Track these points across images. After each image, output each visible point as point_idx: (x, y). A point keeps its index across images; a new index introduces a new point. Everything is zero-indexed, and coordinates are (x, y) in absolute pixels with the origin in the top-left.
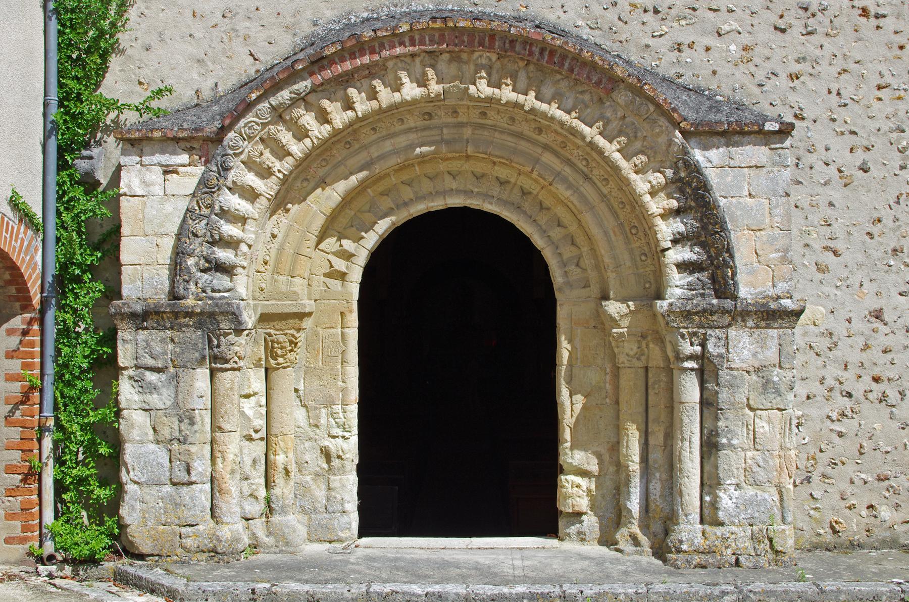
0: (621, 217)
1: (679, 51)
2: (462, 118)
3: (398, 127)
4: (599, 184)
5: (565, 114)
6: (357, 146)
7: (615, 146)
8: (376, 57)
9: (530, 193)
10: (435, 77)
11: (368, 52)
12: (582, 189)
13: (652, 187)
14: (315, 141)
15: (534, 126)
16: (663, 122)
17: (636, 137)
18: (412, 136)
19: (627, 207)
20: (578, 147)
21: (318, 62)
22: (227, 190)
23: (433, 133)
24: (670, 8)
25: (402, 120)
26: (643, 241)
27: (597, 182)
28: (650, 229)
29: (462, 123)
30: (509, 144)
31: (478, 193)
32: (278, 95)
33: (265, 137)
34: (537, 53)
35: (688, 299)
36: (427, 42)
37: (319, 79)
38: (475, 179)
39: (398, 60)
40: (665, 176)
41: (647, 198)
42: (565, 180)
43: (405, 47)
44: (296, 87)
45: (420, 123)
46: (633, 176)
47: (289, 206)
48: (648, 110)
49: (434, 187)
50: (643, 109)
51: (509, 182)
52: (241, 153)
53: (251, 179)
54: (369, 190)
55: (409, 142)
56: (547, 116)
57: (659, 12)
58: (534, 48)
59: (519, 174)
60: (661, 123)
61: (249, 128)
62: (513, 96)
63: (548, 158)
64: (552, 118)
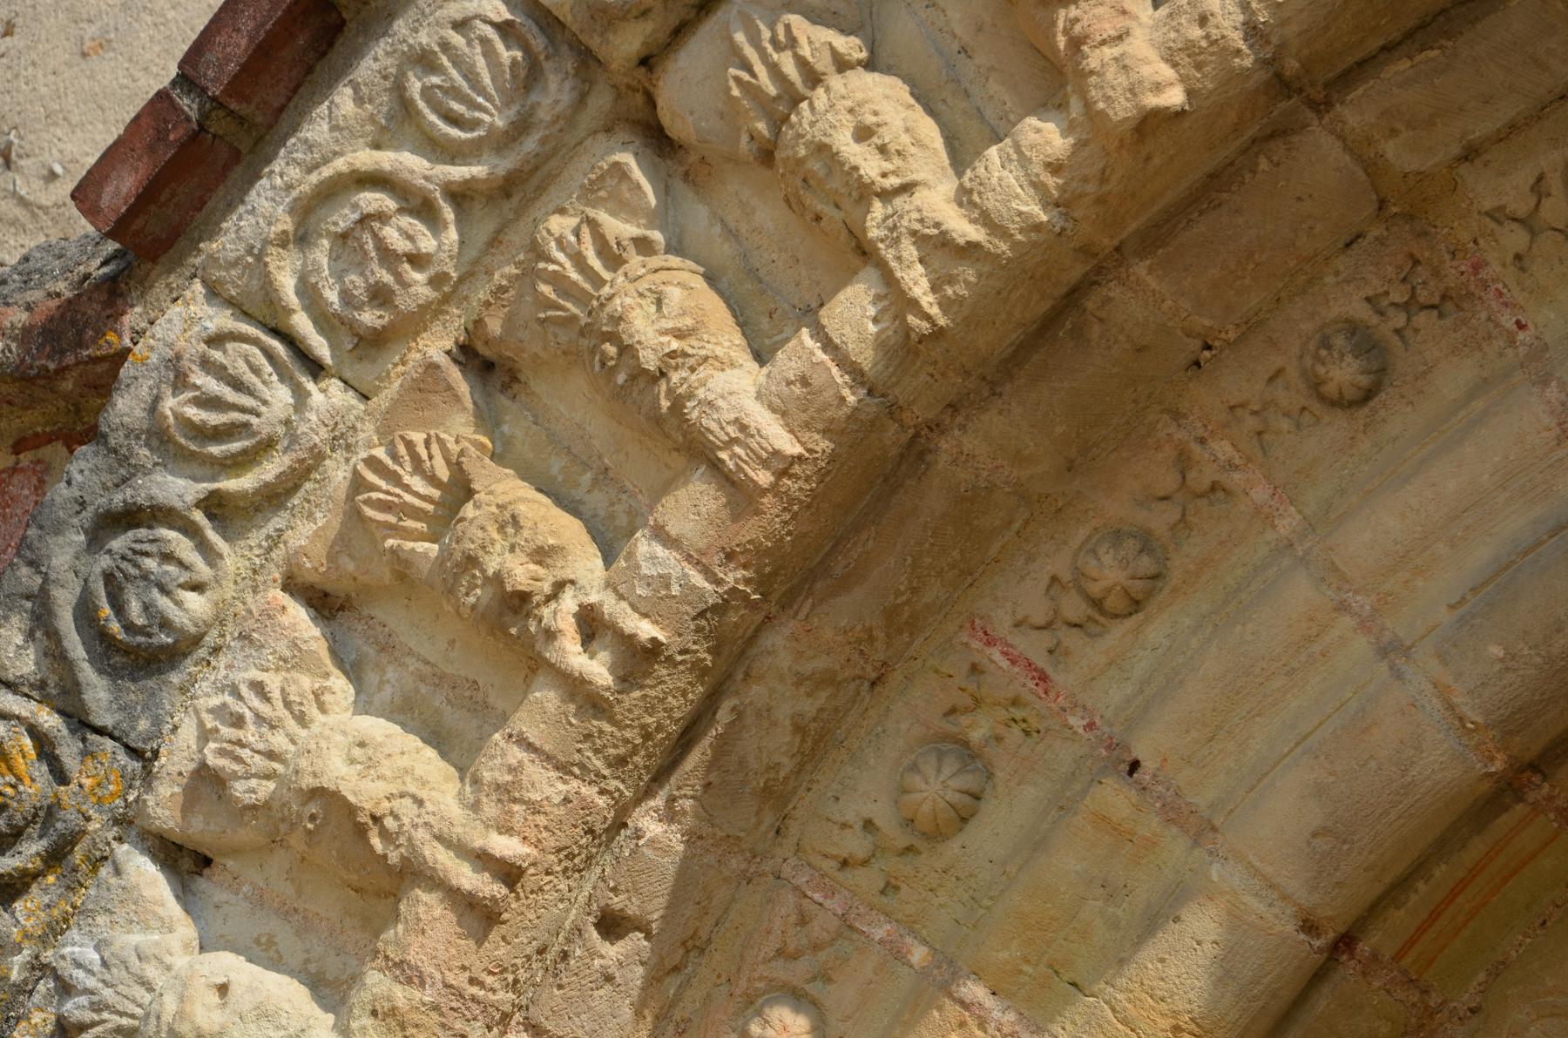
14: (916, 281)
22: (144, 872)
52: (274, 497)
53: (357, 748)
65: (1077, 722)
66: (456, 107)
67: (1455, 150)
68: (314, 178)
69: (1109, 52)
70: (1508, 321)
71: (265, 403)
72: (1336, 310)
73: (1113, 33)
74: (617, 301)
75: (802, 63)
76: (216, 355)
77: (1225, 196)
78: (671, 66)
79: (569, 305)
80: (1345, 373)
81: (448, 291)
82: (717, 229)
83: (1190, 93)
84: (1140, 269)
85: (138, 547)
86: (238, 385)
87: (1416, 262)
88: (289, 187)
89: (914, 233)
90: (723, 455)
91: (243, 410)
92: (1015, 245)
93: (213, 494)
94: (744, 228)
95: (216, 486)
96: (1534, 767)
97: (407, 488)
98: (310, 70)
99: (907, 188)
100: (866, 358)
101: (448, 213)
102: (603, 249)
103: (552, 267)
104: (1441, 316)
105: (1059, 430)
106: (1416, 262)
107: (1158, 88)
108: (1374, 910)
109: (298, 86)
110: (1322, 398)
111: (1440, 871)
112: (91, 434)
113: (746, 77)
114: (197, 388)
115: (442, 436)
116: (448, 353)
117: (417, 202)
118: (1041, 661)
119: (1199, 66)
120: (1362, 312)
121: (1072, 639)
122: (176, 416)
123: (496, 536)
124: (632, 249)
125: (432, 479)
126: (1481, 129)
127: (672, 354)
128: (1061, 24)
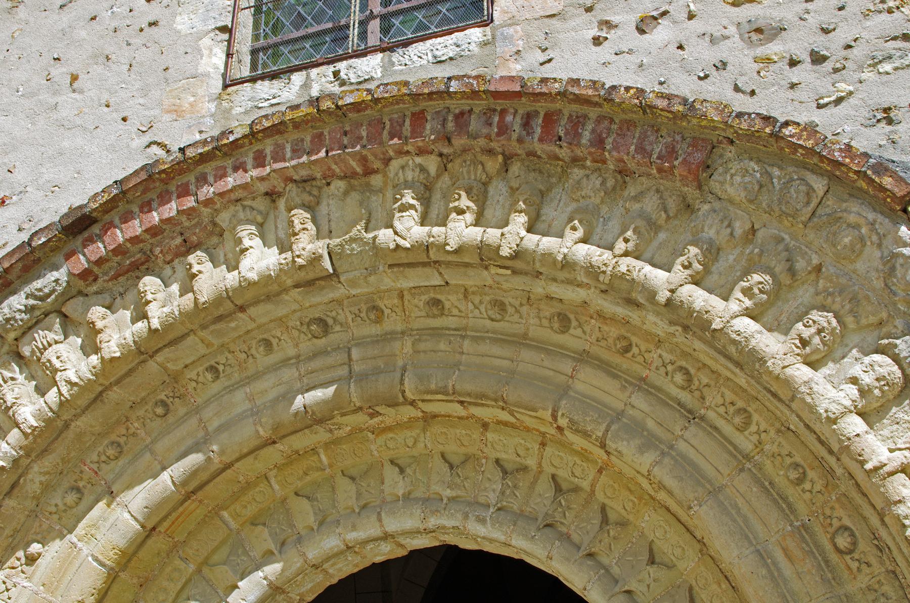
0: (801, 508)
1: (890, 121)
2: (393, 323)
3: (264, 360)
4: (727, 429)
5: (599, 251)
6: (182, 411)
7: (738, 302)
8: (190, 202)
9: (576, 489)
10: (310, 225)
12: (682, 446)
13: (864, 392)
14: (64, 390)
15: (548, 310)
16: (858, 213)
17: (792, 271)
18: (288, 374)
19: (811, 474)
20: (659, 343)
21: (80, 225)
23: (329, 360)
24: (849, 47)
25: (267, 344)
26: (877, 568)
27: (721, 423)
28: (881, 516)
29: (392, 333)
30: (498, 362)
31: (452, 499)
34: (517, 127)
35: (845, 210)
36: (289, 155)
37: (81, 262)
38: (445, 468)
39: (239, 207)
40: (896, 359)
41: (854, 425)
42: (636, 429)
43: (246, 171)
44: (38, 284)
45: (307, 346)
46: (801, 372)
47: (35, 548)
48: (810, 191)
49: (359, 495)
50: (796, 193)
51: (525, 469)
54: (225, 514)
55: (281, 389)
56: (555, 261)
57: (824, 59)
58: (509, 118)
59: (543, 444)
60: (852, 218)
62: (475, 234)
63: (589, 381)
64: (567, 264)
65: (103, 482)
70: (192, 400)
72: (159, 397)
80: (160, 410)
84: (115, 388)
96: (192, 492)
99: (65, 370)
100: (55, 408)
107: (115, 352)
108: (160, 522)
111: (174, 514)
118: (96, 469)
120: (165, 398)
121: (103, 465)
126: (188, 361)
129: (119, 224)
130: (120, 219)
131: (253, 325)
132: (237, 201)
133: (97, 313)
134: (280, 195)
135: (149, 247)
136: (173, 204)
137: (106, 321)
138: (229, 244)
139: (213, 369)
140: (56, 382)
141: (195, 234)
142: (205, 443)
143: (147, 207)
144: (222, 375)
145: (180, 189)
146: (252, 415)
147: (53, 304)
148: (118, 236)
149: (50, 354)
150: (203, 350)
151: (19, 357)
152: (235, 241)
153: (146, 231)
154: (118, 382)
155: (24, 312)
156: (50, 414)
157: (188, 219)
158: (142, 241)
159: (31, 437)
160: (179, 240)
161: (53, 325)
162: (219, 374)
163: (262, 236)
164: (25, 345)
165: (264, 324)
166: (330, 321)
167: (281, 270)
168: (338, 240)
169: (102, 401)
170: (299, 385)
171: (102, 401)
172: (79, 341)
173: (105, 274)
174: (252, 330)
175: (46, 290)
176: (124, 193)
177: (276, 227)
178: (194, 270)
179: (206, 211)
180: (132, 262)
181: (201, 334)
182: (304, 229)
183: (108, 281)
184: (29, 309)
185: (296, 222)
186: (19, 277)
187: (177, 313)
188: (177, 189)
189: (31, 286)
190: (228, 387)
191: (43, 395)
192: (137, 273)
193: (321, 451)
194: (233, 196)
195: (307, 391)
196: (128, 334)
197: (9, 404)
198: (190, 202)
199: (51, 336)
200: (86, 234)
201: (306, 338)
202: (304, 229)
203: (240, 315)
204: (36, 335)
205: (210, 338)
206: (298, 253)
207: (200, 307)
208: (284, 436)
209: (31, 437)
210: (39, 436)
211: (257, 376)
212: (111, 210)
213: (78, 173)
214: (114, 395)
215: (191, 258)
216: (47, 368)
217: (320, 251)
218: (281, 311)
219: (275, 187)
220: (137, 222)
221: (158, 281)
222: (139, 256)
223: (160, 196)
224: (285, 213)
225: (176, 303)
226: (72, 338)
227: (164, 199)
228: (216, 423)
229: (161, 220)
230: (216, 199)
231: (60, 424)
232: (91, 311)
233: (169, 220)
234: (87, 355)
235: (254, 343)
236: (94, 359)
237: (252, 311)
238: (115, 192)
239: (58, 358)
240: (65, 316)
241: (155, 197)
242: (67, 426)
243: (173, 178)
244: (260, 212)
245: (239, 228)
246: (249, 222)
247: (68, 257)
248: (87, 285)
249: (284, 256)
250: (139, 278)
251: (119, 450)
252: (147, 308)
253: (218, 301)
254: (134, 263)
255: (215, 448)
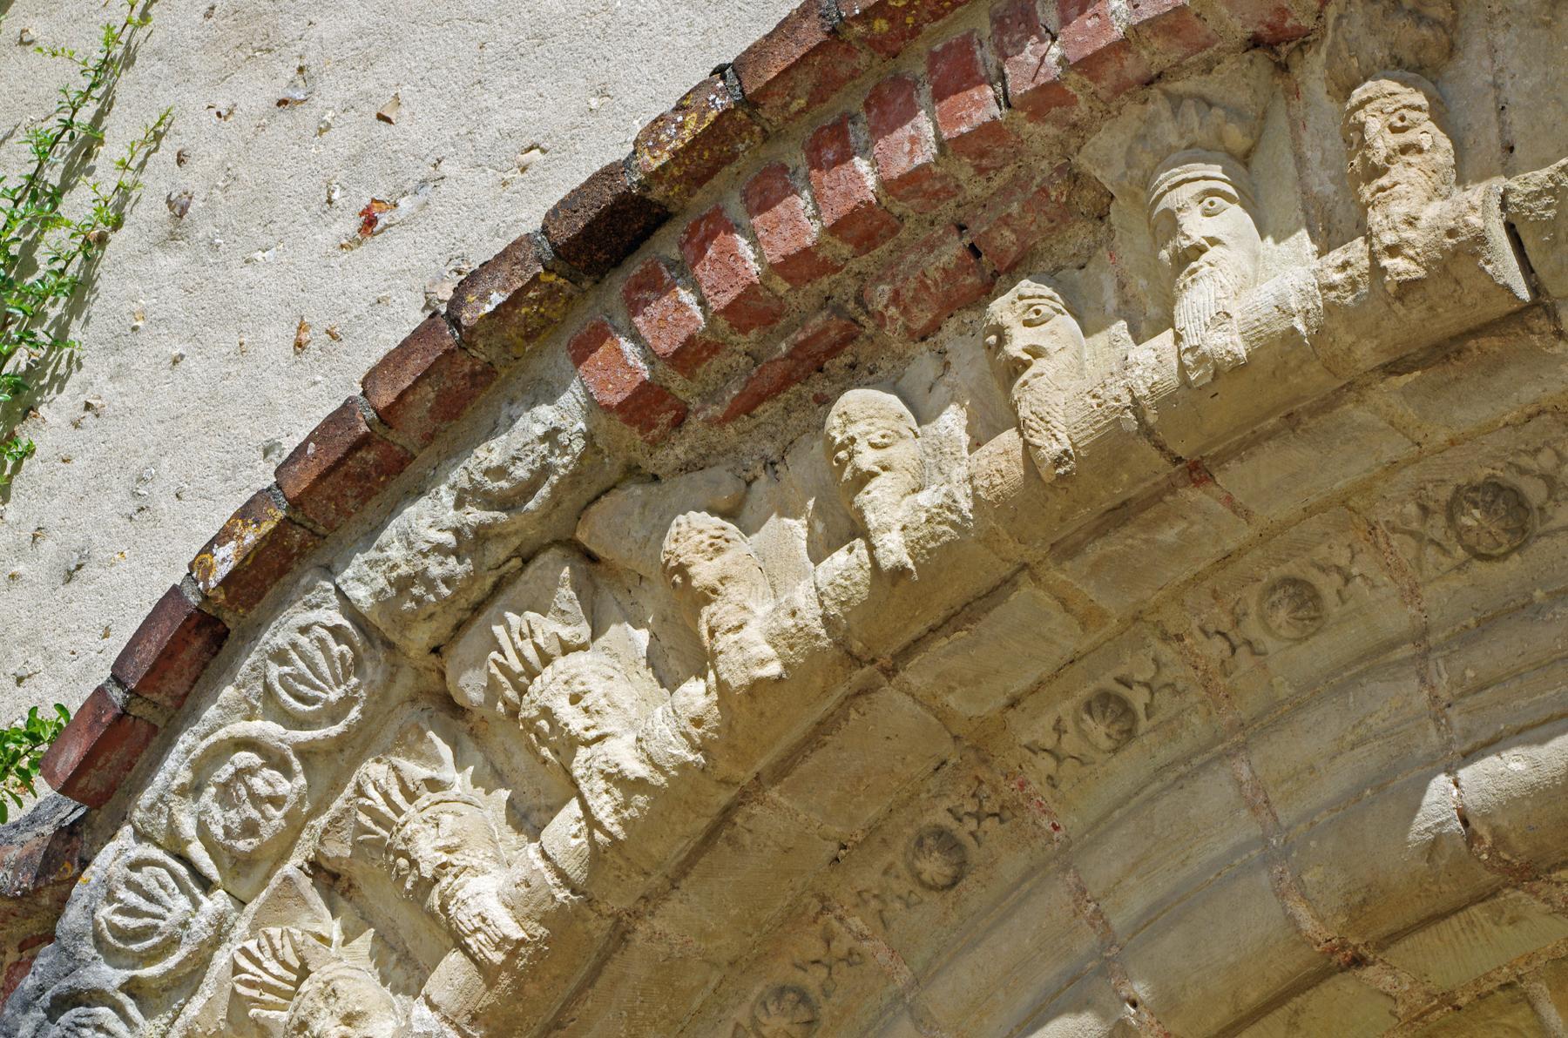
3: (1295, 659)
6: (1012, 864)
8: (981, 107)
10: (1427, 133)
11: (925, 94)
14: (603, 807)
18: (1393, 700)
21: (613, 237)
25: (1302, 594)
32: (390, 533)
33: (338, 849)
37: (628, 361)
39: (1158, 104)
44: (492, 452)
45: (1450, 590)
61: (226, 795)
66: (302, 688)
67: (1003, 700)
68: (204, 744)
69: (732, 637)
70: (1046, 824)
71: (169, 910)
73: (736, 624)
74: (408, 826)
75: (537, 647)
76: (136, 876)
77: (828, 738)
78: (453, 652)
79: (378, 829)
80: (934, 866)
81: (296, 824)
82: (488, 769)
83: (786, 666)
84: (773, 793)
85: (78, 1020)
86: (150, 898)
87: (981, 782)
88: (188, 752)
89: (602, 772)
90: (469, 941)
91: (154, 916)
92: (670, 779)
93: (133, 979)
94: (506, 768)
95: (136, 972)
97: (265, 970)
98: (205, 666)
99: (600, 738)
101: (297, 765)
102: (404, 789)
103: (369, 802)
104: (1002, 821)
105: (733, 912)
106: (981, 782)
107: (763, 663)
109: (197, 678)
110: (923, 884)
112: (50, 937)
113: (501, 659)
114: (121, 901)
115: (293, 930)
116: (301, 868)
117: (276, 759)
119: (791, 647)
120: (948, 822)
122: (109, 923)
123: (321, 1005)
124: (423, 787)
125: (284, 964)
126: (1018, 686)
127: (443, 866)
128: (705, 617)
129: (744, 220)
130: (746, 197)
131: (1246, 533)
132: (1149, 83)
133: (693, 535)
134: (1303, 40)
135: (852, 286)
136: (924, 124)
137: (727, 557)
138: (1131, 242)
139: (1111, 705)
140: (574, 783)
141: (1006, 221)
142: (1104, 970)
143: (831, 145)
144: (1143, 724)
145: (942, 67)
146: (1267, 862)
147: (546, 516)
148: (747, 256)
149: (549, 689)
150: (1067, 638)
151: (450, 709)
152: (1153, 229)
153: (835, 229)
154: (781, 771)
155: (455, 552)
156: (562, 895)
157: (981, 171)
158: (828, 268)
159: (505, 980)
160: (952, 250)
161: (551, 592)
162: (1134, 719)
163: (1250, 201)
164: (463, 667)
165: (1284, 527)
166: (1534, 491)
167: (1330, 308)
168: (1543, 174)
169: (732, 841)
170: (1434, 738)
171: (732, 841)
172: (642, 637)
173: (709, 397)
174: (1241, 552)
175: (521, 472)
176: (750, 103)
177: (1300, 161)
178: (1015, 349)
179: (1039, 134)
180: (799, 347)
181: (1057, 575)
182: (1405, 149)
183: (722, 422)
184: (471, 542)
185: (1374, 125)
186: (430, 438)
187: (965, 505)
188: (932, 70)
189: (470, 462)
190: (1170, 766)
191: (535, 835)
192: (819, 385)
193: (1540, 989)
194: (1132, 67)
195: (1469, 757)
196: (802, 596)
197: (427, 871)
198: (981, 107)
199: (547, 628)
200: (635, 267)
201: (1447, 562)
202: (1405, 149)
203: (1193, 495)
204: (498, 630)
205: (1090, 590)
206: (1389, 238)
207: (1047, 474)
208: (1394, 937)
209: (505, 980)
210: (533, 972)
211: (1274, 718)
212: (713, 172)
213: (602, 93)
214: (776, 816)
215: (1002, 308)
216: (542, 739)
217: (1475, 220)
218: (1342, 471)
219: (1283, 12)
220: (802, 202)
221: (894, 401)
222: (819, 320)
223: (876, 101)
224: (1329, 104)
225: (959, 472)
226: (617, 632)
227: (889, 107)
228: (1136, 901)
229: (886, 185)
230: (1073, 83)
231: (598, 928)
232: (673, 530)
233: (914, 178)
234: (669, 682)
235: (1251, 596)
236: (696, 693)
237: (1236, 477)
238: (721, 102)
239: (575, 699)
240: (591, 558)
241: (857, 106)
242: (621, 935)
243: (916, 31)
244: (1236, 113)
245: (1165, 178)
246: (1197, 151)
247: (582, 351)
248: (653, 443)
249: (1337, 256)
250: (826, 401)
251: (803, 1014)
252: (862, 498)
253: (1110, 446)
254: (802, 351)
255: (1140, 989)
